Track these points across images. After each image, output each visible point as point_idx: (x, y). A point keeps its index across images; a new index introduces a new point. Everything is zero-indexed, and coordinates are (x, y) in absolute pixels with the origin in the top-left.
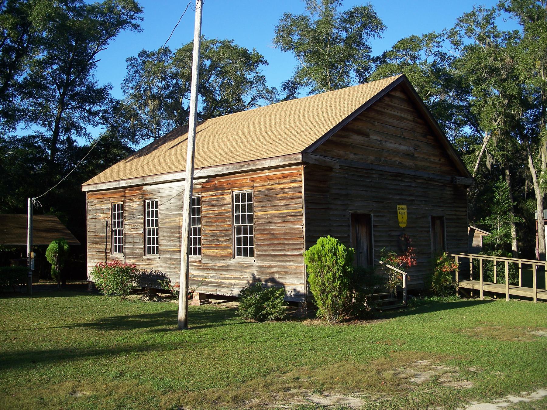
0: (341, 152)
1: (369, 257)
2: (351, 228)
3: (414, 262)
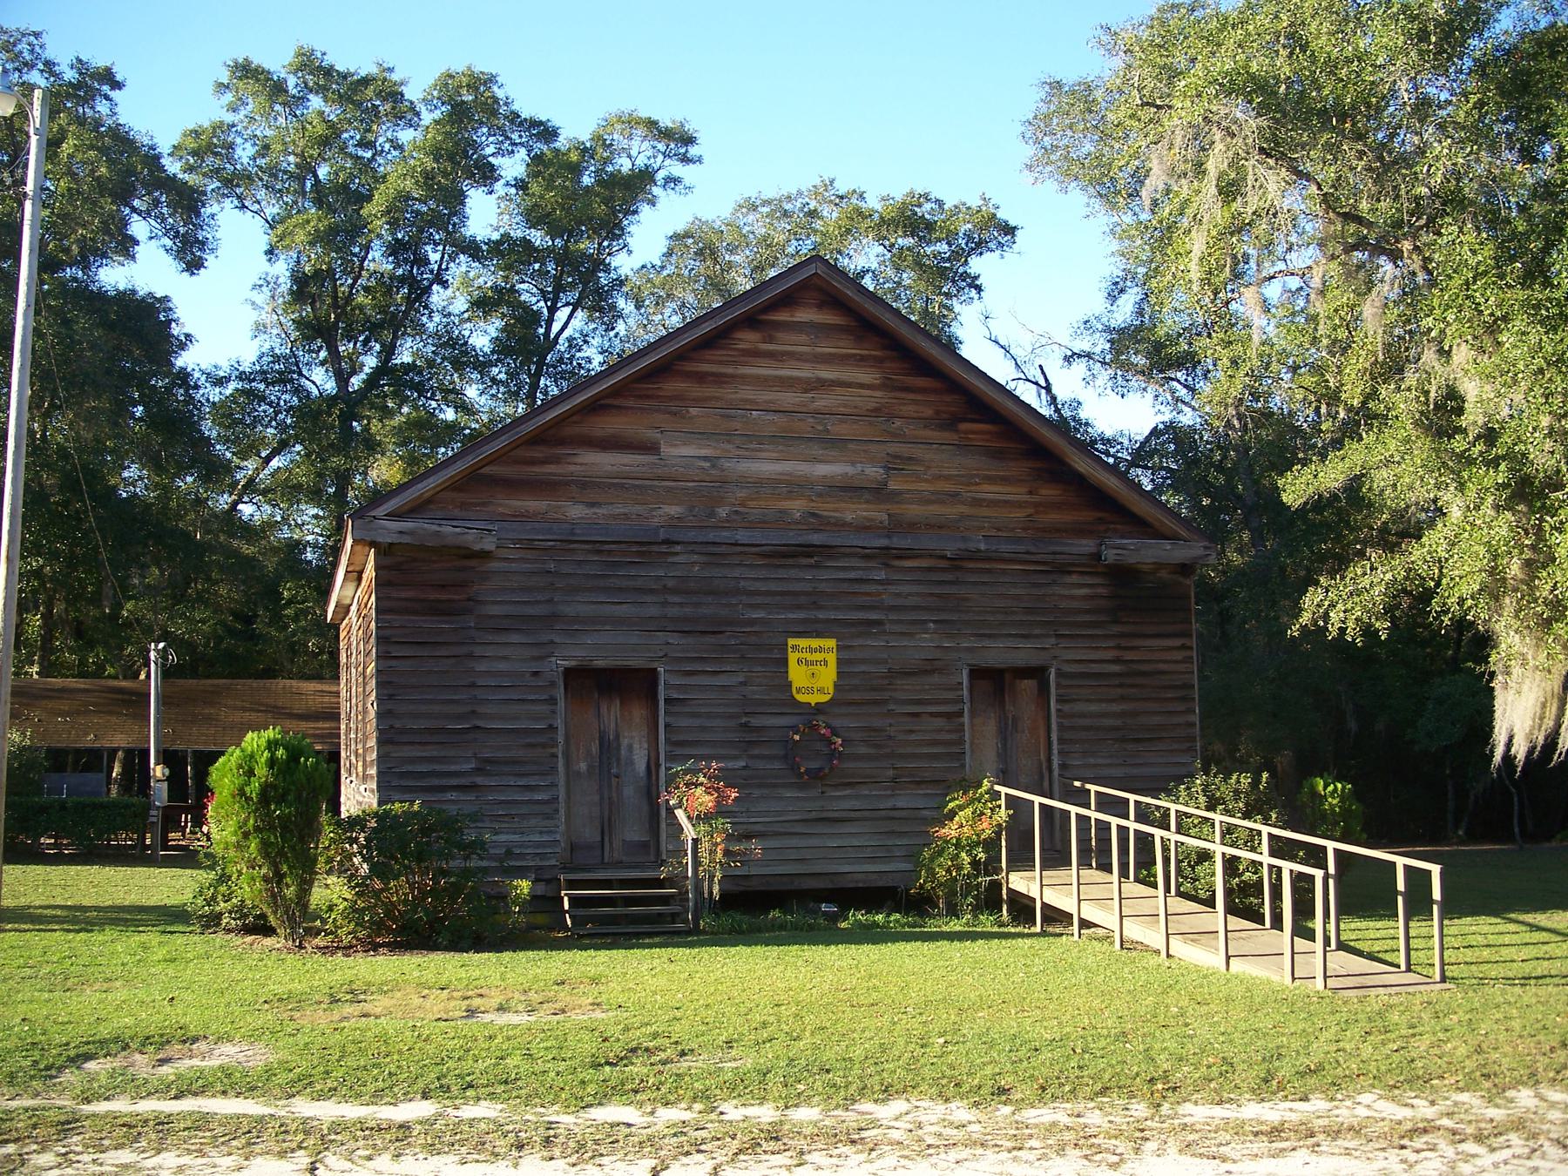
2: (561, 704)
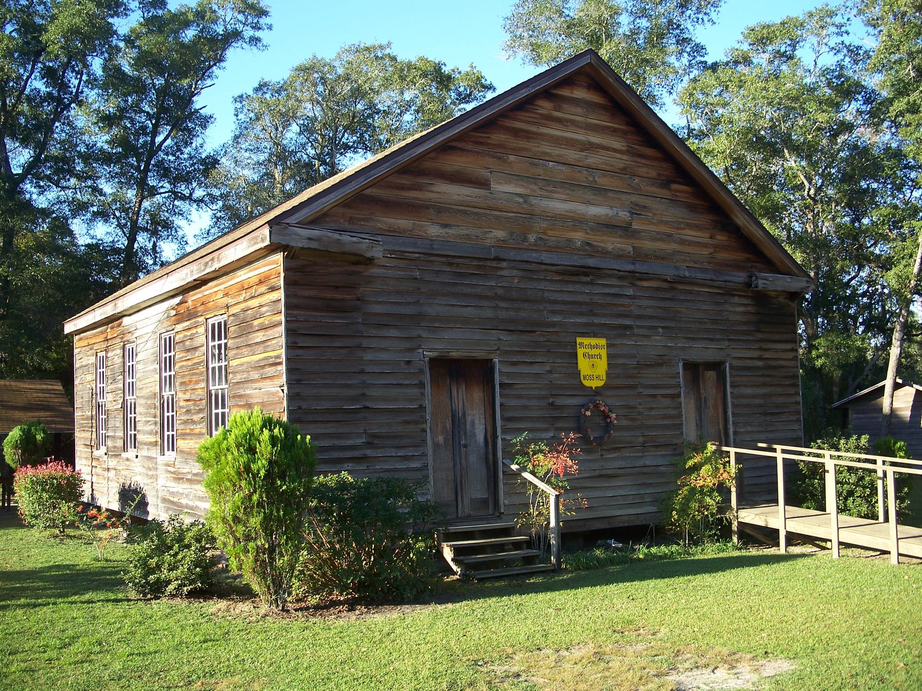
0: (403, 223)
3: (571, 467)
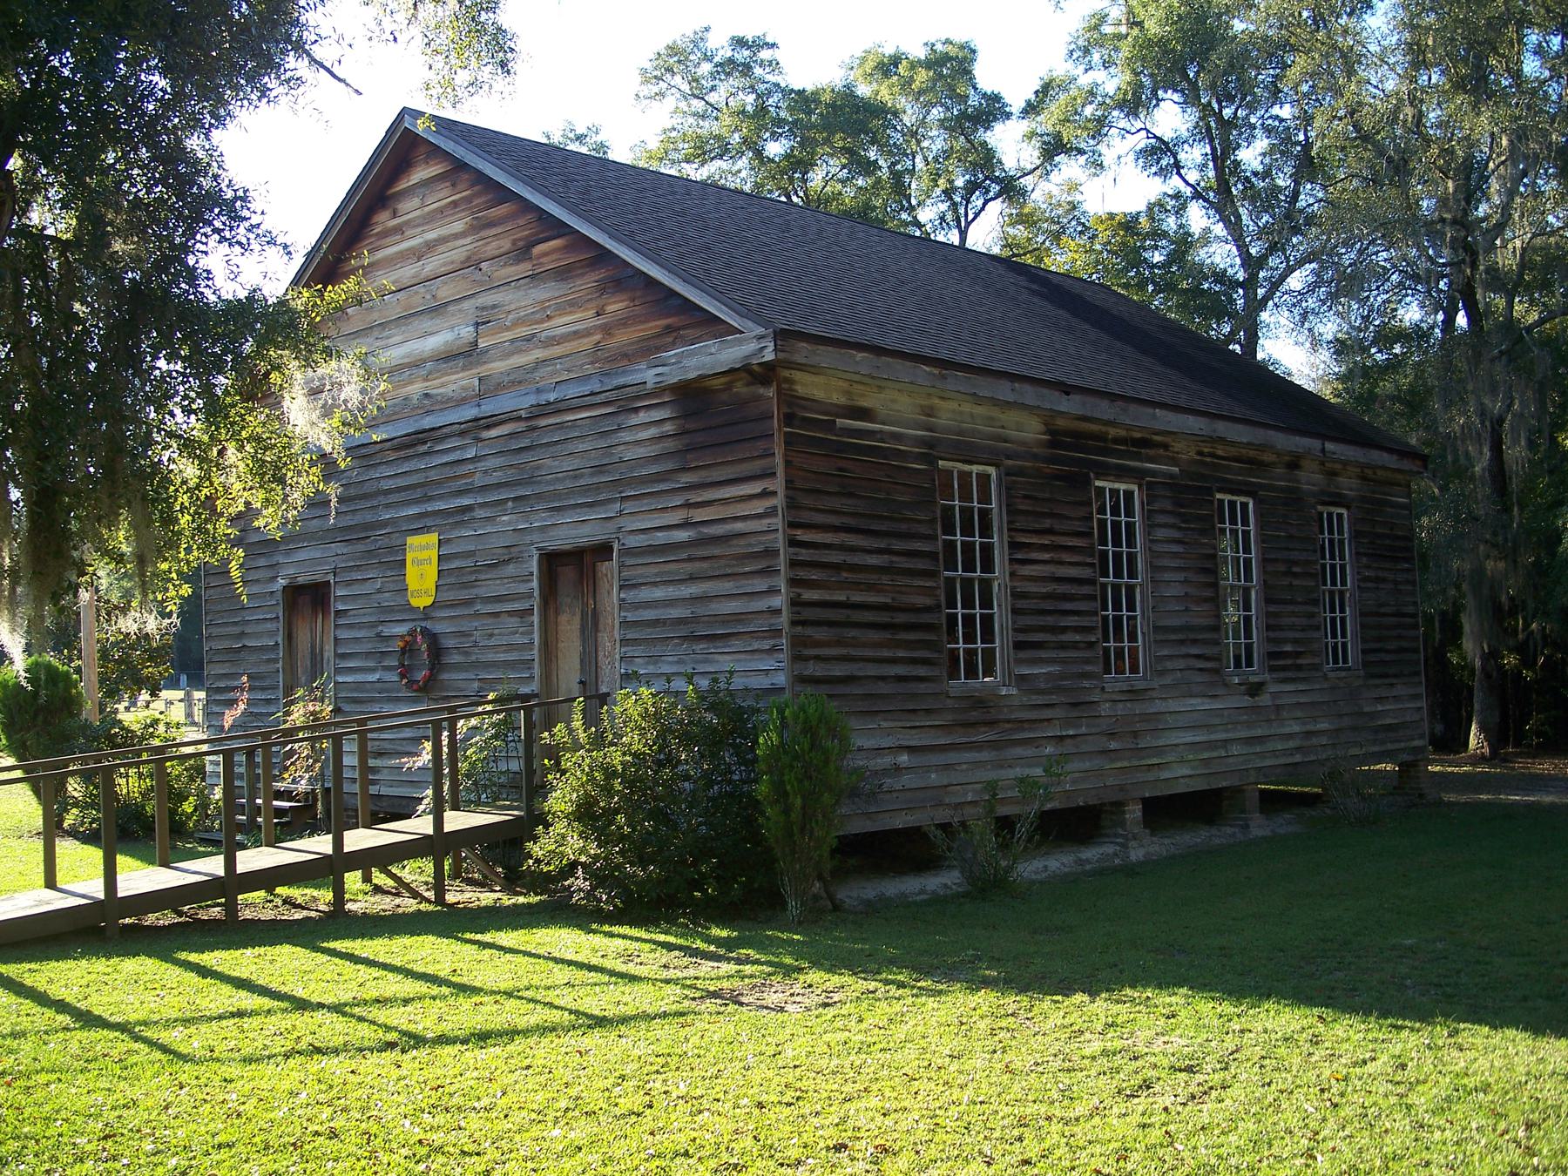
1: (1173, 637)
